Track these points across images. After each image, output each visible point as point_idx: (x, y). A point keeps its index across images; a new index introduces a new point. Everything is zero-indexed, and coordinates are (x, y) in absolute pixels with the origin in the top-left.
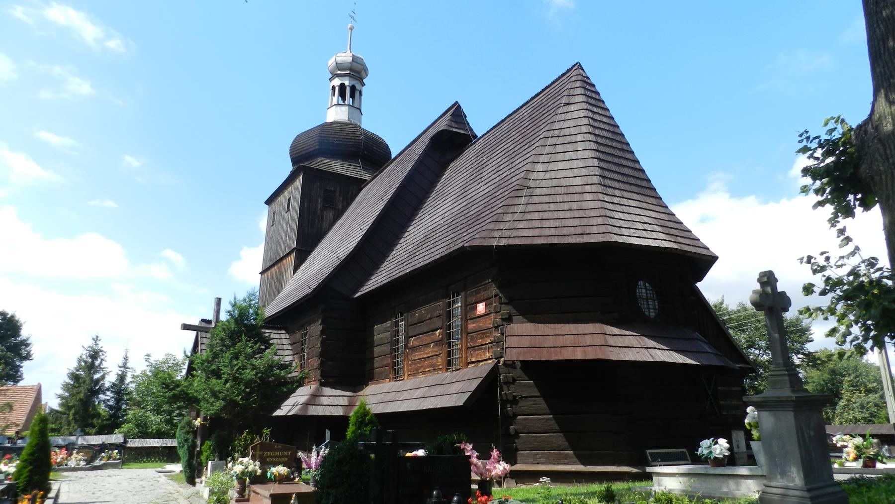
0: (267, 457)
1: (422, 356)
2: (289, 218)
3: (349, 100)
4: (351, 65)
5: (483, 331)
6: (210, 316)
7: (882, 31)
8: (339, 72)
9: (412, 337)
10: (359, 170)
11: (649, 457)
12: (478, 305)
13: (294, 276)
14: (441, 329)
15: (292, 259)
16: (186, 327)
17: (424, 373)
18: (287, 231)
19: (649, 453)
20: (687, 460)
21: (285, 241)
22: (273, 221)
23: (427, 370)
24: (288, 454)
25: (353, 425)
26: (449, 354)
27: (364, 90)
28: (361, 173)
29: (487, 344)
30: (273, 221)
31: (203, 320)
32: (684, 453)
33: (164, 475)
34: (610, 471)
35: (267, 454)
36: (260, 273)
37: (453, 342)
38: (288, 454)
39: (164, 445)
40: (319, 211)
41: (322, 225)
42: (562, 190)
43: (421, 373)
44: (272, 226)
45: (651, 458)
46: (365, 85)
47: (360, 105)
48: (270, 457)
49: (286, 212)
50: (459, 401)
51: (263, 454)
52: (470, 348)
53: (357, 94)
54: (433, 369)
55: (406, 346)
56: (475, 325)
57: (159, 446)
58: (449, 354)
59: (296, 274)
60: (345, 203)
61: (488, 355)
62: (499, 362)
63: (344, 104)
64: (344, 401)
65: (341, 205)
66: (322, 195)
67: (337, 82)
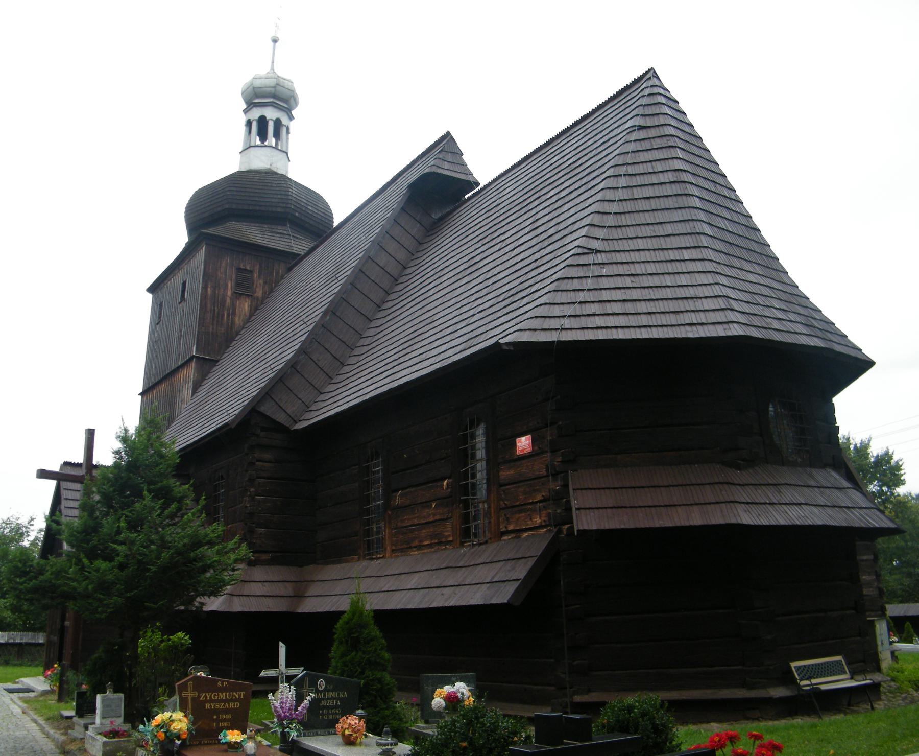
0: (206, 701)
1: (416, 521)
2: (183, 311)
3: (271, 141)
4: (275, 90)
5: (529, 482)
6: (79, 458)
8: (257, 101)
10: (289, 240)
11: (796, 674)
12: (517, 440)
13: (193, 398)
14: (449, 478)
15: (190, 373)
16: (43, 474)
17: (420, 547)
18: (181, 331)
19: (795, 667)
20: (845, 673)
21: (179, 345)
22: (160, 317)
23: (425, 543)
24: (240, 696)
25: (341, 643)
26: (466, 518)
27: (293, 125)
28: (290, 244)
29: (536, 502)
30: (160, 317)
31: (67, 464)
32: (839, 662)
33: (20, 698)
34: (740, 697)
35: (206, 696)
36: (139, 394)
37: (472, 499)
38: (240, 696)
39: (11, 641)
40: (228, 301)
41: (233, 322)
43: (415, 547)
44: (157, 324)
45: (799, 675)
46: (294, 118)
47: (287, 147)
48: (211, 701)
49: (180, 303)
50: (503, 596)
51: (199, 696)
52: (504, 509)
53: (284, 130)
54: (436, 541)
55: (387, 505)
56: (512, 472)
57: (4, 642)
58: (466, 518)
59: (196, 395)
60: (267, 288)
61: (538, 520)
62: (560, 531)
63: (262, 145)
64: (288, 590)
65: (261, 292)
66: (234, 276)
67: (256, 114)
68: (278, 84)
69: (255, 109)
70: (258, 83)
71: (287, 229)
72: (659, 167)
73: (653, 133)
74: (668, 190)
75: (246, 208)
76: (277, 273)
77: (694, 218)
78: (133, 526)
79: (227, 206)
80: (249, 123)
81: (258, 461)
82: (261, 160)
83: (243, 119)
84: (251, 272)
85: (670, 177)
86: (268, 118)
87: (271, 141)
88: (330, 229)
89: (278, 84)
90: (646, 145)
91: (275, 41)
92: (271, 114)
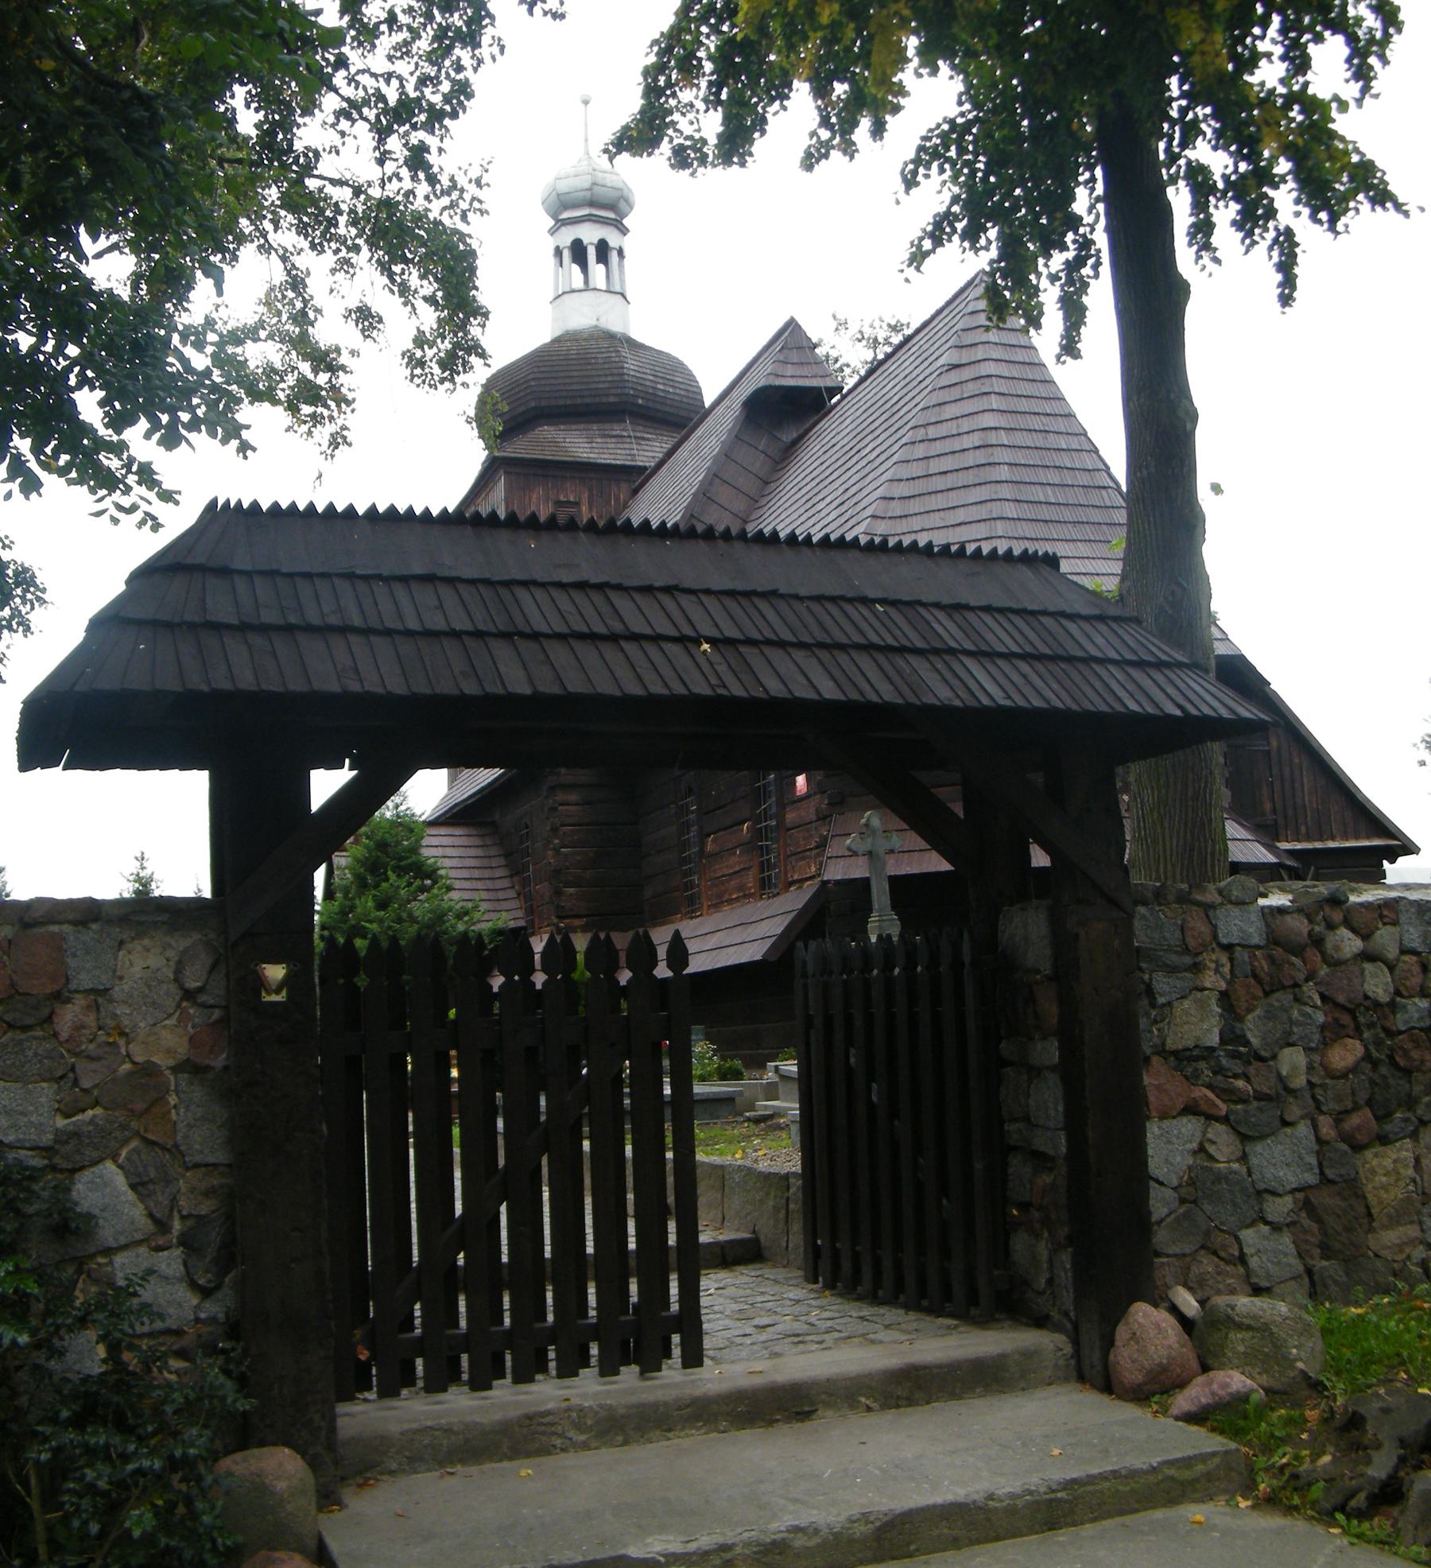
7: (407, 858)
9: (709, 835)
17: (730, 901)
27: (628, 243)
42: (1053, 477)
53: (614, 257)
67: (567, 237)
68: (594, 184)
69: (563, 229)
70: (564, 186)
71: (627, 428)
72: (966, 425)
73: (966, 374)
74: (970, 459)
75: (561, 402)
76: (617, 499)
77: (994, 497)
78: (382, 905)
79: (533, 404)
80: (558, 252)
81: (561, 805)
82: (583, 315)
83: (550, 244)
84: (577, 504)
85: (976, 439)
86: (585, 242)
87: (598, 271)
88: (697, 413)
89: (594, 184)
90: (955, 393)
91: (586, 103)
92: (590, 234)
